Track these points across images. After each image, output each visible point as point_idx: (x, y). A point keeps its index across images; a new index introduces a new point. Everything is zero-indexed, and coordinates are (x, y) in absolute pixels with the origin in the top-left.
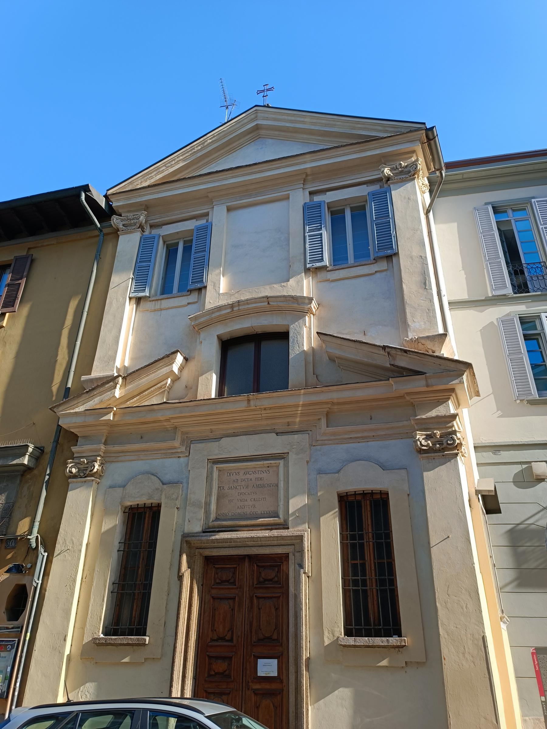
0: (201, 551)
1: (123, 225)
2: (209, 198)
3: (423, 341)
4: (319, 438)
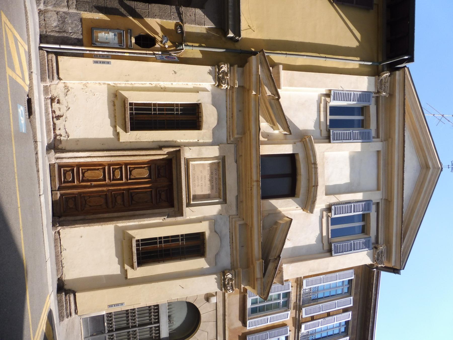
0: (175, 158)
1: (382, 79)
2: (388, 139)
3: (281, 273)
4: (234, 219)
